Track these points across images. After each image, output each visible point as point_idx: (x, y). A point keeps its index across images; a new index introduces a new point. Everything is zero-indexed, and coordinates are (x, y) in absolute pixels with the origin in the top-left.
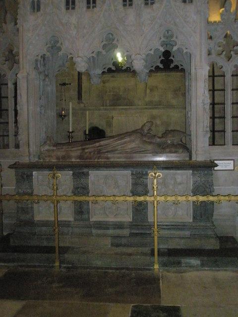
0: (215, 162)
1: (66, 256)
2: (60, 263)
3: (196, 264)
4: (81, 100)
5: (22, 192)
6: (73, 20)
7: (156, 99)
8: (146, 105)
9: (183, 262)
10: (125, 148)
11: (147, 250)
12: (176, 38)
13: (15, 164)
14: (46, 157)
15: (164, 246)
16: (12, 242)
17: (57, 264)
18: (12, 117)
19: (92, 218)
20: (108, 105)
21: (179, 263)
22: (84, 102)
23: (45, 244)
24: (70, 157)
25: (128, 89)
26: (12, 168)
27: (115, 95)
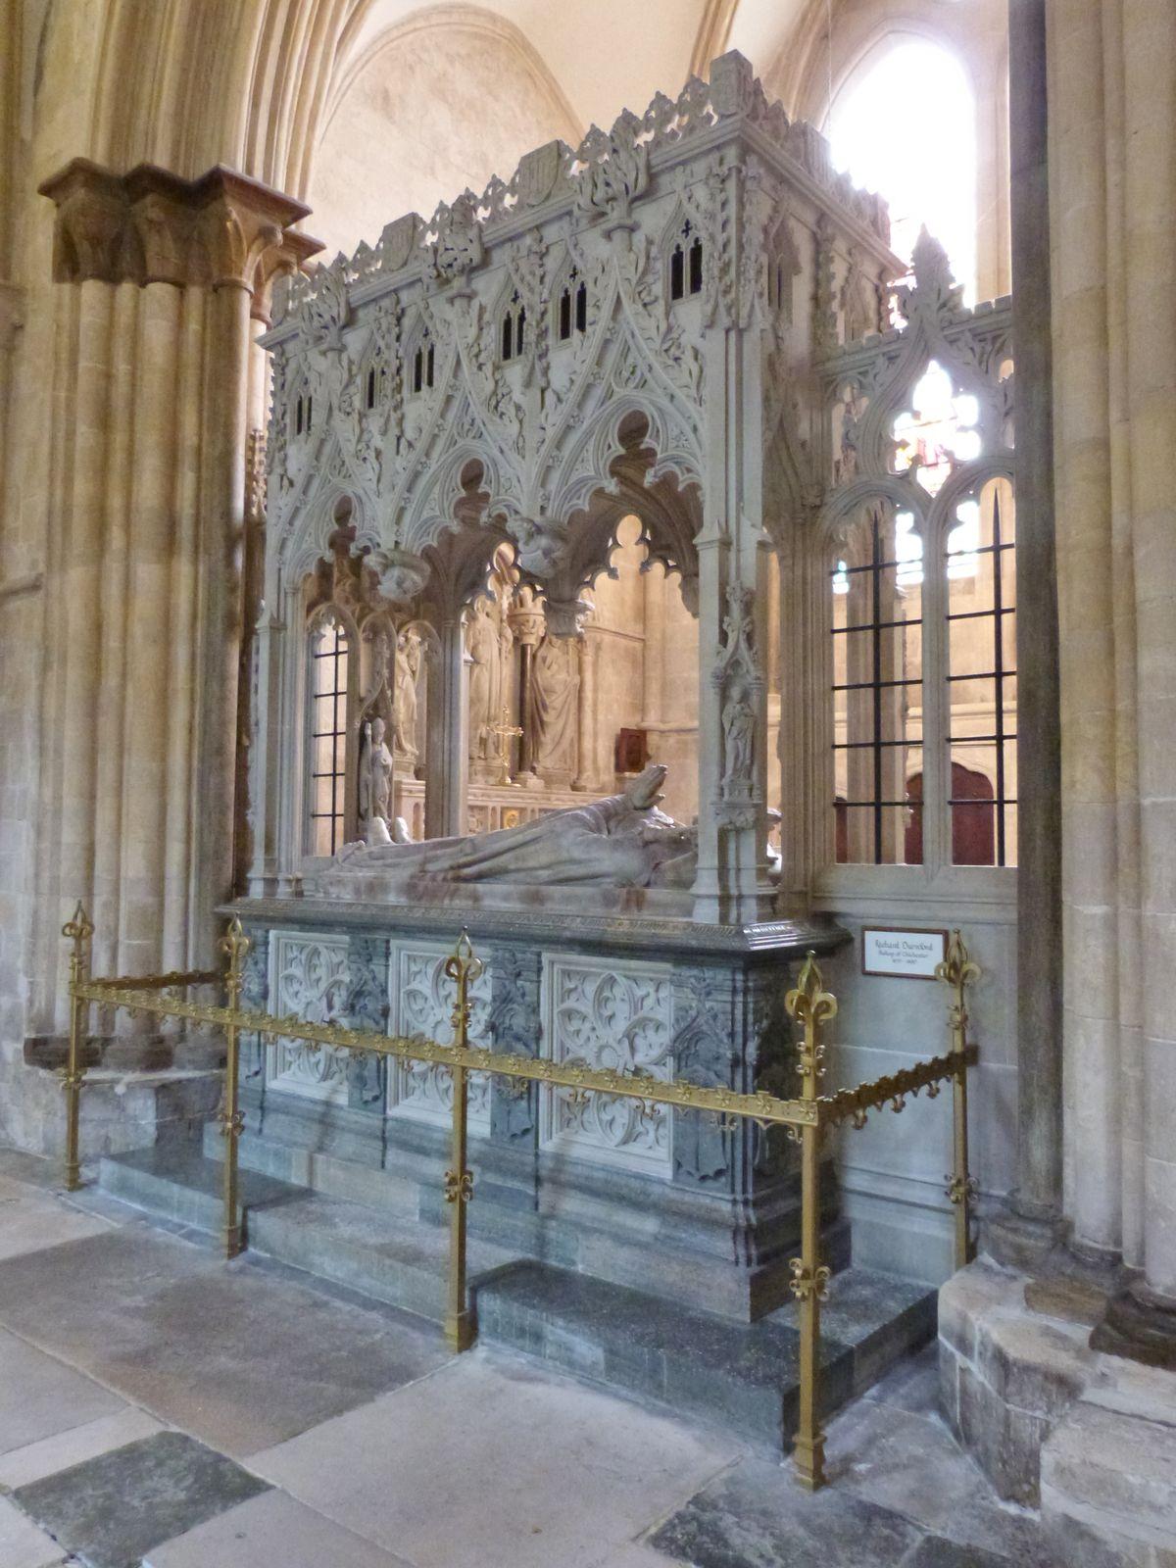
3: (589, 1362)
19: (396, 1102)
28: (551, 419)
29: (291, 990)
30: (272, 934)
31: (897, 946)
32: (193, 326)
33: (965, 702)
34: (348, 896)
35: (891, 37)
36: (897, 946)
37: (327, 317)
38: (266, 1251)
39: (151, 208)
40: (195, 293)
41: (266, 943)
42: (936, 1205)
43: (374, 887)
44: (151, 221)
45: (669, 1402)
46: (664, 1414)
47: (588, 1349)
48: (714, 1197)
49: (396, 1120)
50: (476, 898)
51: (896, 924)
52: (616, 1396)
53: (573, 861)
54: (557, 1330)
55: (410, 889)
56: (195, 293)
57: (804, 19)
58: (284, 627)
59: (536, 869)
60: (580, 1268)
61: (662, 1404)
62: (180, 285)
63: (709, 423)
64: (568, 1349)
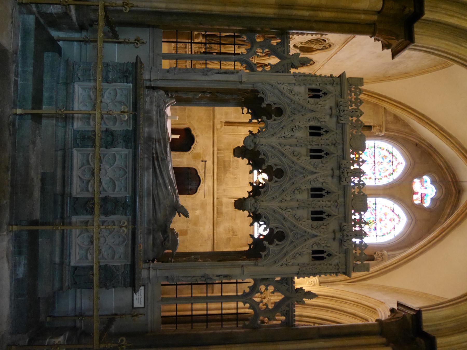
0: (142, 288)
1: (30, 121)
2: (20, 115)
3: (18, 272)
4: (225, 125)
5: (109, 70)
6: (299, 134)
7: (224, 209)
8: (217, 198)
9: (21, 258)
10: (159, 189)
11: (29, 123)
12: (277, 245)
13: (142, 63)
14: (151, 98)
15: (29, 104)
16: (48, 57)
17: (19, 111)
18: (128, 240)
19: (78, 151)
20: (218, 156)
21: (20, 254)
22: (223, 128)
23: (46, 94)
24: (150, 125)
25: (236, 178)
26: (137, 59)
27: (229, 164)
28: (288, 213)
29: (111, 92)
30: (131, 85)
31: (140, 295)
32: (363, 17)
33: (217, 184)
34: (147, 106)
35: (410, 163)
36: (140, 295)
37: (342, 114)
38: (18, 126)
39: (410, 9)
40: (375, 18)
41: (127, 83)
42: (77, 307)
43: (149, 119)
44: (405, 8)
45: (14, 300)
46: (11, 299)
47: (21, 271)
48: (69, 280)
49: (72, 152)
50: (148, 168)
51: (146, 294)
52: (11, 284)
53: (160, 204)
54: (23, 261)
55: (150, 138)
56: (375, 18)
57: (424, 140)
58: (241, 84)
59: (157, 190)
60: (40, 240)
61: (13, 298)
62: (379, 13)
63: (285, 223)
64: (19, 265)
